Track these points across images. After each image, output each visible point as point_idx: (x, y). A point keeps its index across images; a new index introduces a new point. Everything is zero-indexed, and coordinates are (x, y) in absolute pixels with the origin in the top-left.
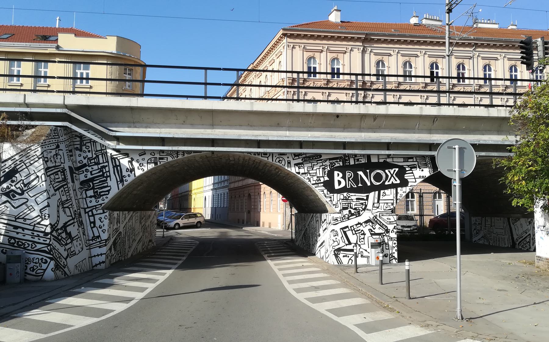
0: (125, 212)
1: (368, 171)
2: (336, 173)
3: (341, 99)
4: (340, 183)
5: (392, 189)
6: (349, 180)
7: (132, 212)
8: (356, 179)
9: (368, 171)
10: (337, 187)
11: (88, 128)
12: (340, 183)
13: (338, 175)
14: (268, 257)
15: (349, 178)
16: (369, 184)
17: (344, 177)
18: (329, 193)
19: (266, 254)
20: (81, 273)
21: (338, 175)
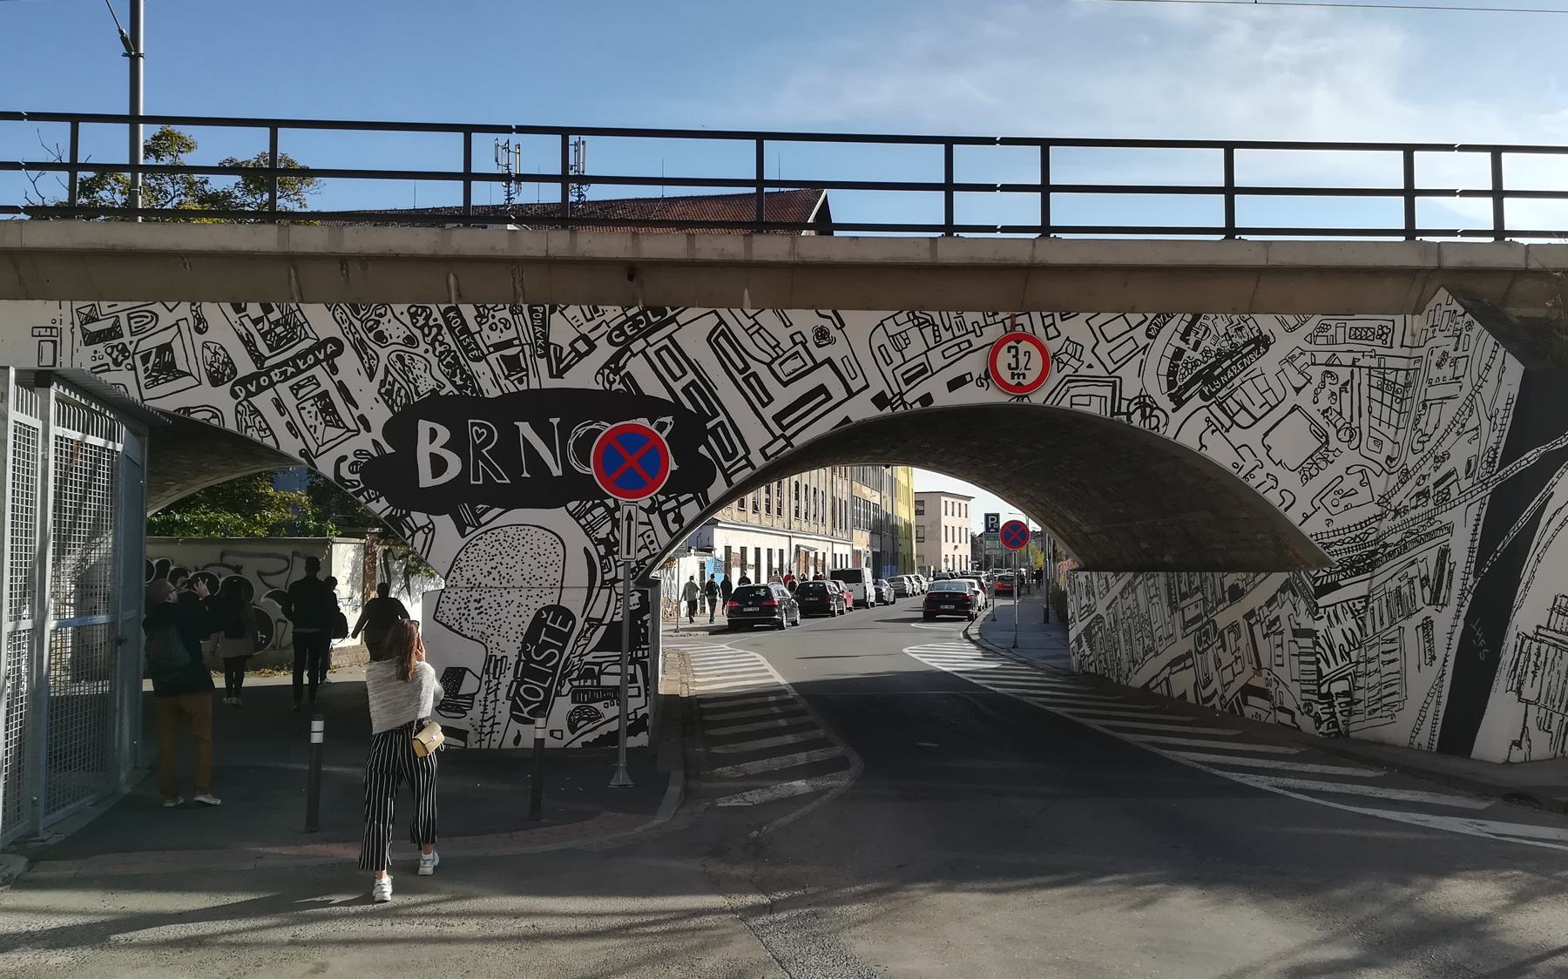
0: (1103, 574)
1: (555, 421)
2: (424, 426)
3: (584, 919)
4: (439, 465)
5: (822, 471)
6: (478, 455)
7: (1129, 576)
8: (510, 445)
9: (555, 421)
10: (426, 479)
11: (45, 460)
12: (439, 465)
13: (433, 435)
14: (784, 692)
15: (478, 448)
16: (557, 472)
17: (457, 444)
18: (1291, 320)
19: (792, 701)
20: (1052, 310)
21: (433, 435)
